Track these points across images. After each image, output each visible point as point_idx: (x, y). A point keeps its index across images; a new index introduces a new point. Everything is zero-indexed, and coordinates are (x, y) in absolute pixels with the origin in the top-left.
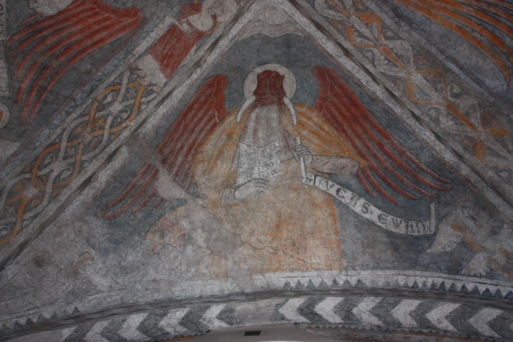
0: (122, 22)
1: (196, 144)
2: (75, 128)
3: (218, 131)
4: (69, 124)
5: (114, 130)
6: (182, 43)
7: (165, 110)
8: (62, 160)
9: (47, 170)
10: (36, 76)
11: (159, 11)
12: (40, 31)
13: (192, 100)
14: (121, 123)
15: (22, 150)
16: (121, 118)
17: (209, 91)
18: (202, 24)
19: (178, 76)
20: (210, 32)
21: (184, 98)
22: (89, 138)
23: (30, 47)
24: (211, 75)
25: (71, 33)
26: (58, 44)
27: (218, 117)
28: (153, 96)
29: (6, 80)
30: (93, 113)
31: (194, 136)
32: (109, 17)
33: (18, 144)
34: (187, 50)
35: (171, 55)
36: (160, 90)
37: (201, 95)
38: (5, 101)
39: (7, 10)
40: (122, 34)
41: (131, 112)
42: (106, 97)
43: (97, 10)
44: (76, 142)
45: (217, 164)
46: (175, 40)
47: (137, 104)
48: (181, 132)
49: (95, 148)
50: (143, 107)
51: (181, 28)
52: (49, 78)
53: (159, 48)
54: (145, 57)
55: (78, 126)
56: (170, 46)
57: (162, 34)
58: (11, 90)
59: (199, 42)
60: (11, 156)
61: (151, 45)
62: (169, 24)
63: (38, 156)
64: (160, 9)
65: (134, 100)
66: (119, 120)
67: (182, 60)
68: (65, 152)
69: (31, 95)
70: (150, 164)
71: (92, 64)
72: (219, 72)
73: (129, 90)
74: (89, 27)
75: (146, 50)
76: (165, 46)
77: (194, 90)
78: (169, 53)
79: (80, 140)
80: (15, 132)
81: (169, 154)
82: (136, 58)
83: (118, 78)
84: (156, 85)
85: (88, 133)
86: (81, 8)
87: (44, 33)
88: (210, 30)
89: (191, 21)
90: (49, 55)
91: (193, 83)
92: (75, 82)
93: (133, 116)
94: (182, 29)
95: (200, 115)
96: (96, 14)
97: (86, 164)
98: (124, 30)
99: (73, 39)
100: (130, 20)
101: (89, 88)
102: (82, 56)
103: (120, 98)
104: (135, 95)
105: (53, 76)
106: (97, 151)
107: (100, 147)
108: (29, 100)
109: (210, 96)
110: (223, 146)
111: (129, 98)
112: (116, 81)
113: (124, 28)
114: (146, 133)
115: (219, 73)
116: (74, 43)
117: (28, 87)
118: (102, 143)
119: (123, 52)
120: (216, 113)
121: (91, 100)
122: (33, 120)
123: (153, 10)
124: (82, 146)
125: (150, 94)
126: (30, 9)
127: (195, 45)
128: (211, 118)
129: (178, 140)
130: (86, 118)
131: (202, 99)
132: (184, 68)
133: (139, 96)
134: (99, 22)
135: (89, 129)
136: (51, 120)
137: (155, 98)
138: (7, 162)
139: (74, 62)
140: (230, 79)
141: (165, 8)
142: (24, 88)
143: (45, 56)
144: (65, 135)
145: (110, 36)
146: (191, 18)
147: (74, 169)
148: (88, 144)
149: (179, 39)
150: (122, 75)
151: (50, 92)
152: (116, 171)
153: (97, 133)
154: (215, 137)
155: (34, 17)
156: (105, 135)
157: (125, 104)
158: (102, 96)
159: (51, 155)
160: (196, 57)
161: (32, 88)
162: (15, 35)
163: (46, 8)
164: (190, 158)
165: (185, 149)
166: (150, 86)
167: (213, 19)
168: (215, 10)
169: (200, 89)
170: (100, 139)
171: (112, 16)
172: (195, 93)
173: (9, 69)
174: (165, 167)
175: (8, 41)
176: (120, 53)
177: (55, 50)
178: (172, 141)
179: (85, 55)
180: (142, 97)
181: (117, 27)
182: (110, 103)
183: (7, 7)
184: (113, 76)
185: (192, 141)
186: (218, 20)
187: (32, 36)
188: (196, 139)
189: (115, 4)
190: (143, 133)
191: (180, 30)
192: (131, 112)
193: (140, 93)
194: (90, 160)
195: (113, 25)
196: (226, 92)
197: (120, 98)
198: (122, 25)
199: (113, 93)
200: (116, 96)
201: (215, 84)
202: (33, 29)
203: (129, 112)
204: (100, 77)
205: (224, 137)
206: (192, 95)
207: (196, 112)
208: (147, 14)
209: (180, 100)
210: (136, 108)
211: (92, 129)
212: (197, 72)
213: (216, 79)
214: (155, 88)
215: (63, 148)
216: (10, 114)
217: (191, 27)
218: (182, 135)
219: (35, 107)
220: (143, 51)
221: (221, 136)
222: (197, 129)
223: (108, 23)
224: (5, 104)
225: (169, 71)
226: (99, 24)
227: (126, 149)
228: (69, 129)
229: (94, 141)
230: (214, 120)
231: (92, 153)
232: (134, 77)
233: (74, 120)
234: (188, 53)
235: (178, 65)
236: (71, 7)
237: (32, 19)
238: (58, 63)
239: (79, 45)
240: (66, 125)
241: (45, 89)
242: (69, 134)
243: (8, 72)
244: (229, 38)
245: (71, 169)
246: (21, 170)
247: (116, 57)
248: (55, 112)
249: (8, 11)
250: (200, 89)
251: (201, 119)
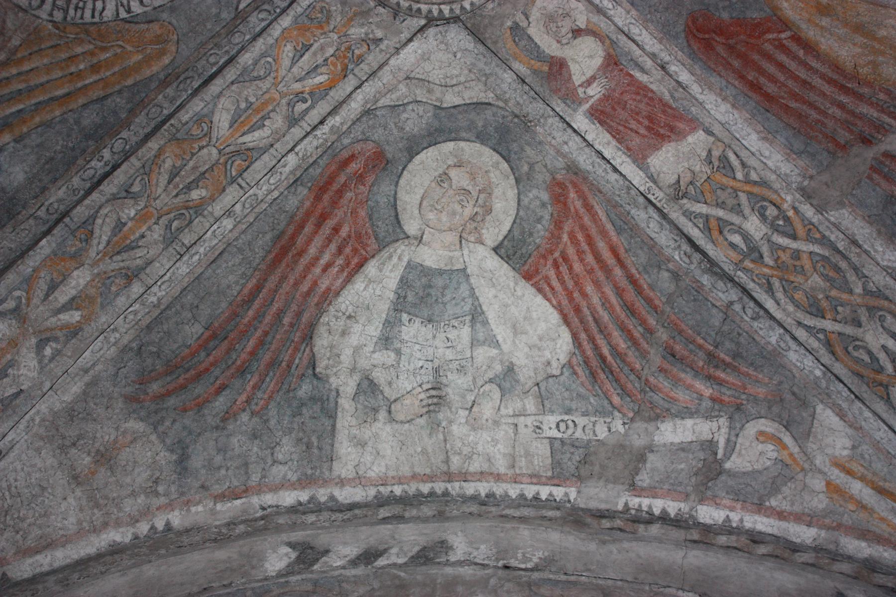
0: (576, 211)
1: (835, 77)
2: (797, 306)
3: (810, 33)
4: (788, 315)
5: (801, 232)
6: (626, 97)
7: (754, 136)
8: (861, 330)
9: (882, 356)
10: (688, 369)
11: (553, 141)
12: (603, 359)
13: (736, 83)
14: (787, 219)
15: (831, 401)
16: (777, 218)
17: (720, 49)
18: (591, 57)
19: (693, 109)
20: (608, 41)
21: (731, 99)
22: (816, 280)
23: (632, 377)
24: (685, 44)
25: (603, 304)
26: (623, 328)
27: (780, 32)
28: (732, 157)
29: (698, 421)
30: (766, 271)
31: (817, 81)
32: (569, 235)
33: (820, 408)
34: (642, 90)
35: (650, 118)
36: (720, 144)
37: (728, 65)
38: (738, 425)
39: (566, 414)
40: (599, 212)
41: (764, 199)
42: (733, 245)
43: (557, 254)
44: (824, 304)
45: (886, 37)
46: (619, 110)
47: (747, 188)
48: (805, 107)
49: (837, 269)
50: (754, 176)
51: (595, 98)
52: (691, 346)
53: (636, 142)
54: (652, 169)
55: (792, 299)
56: (632, 122)
57: (608, 136)
58: (717, 413)
59: (625, 64)
60: (845, 421)
61: (629, 156)
62: (587, 120)
63: (853, 372)
64: (549, 139)
65: (740, 193)
66: (781, 223)
67: (661, 100)
68: (846, 323)
69: (724, 381)
70: (870, 169)
71: (659, 268)
72: (680, 28)
73: (720, 201)
74: (591, 272)
75: (638, 166)
76: (631, 130)
77: (714, 79)
78: (646, 122)
79: (820, 296)
80: (795, 412)
81: (851, 132)
82: (654, 186)
83: (695, 221)
84: (710, 151)
85: (807, 280)
86: (555, 283)
87: (606, 351)
88: (603, 43)
89: (584, 79)
90: (646, 346)
91: (699, 81)
92: (695, 300)
93: (774, 197)
94: (598, 96)
95: (771, 69)
96: (565, 259)
97: (871, 287)
98: (592, 207)
99: (614, 299)
100: (572, 195)
101: (706, 276)
102: (645, 286)
103: (736, 219)
104: (730, 190)
105: (687, 339)
106: (843, 265)
107: (836, 259)
108: (733, 384)
109: (731, 48)
110: (846, 24)
111: (735, 202)
112: (701, 226)
113: (589, 208)
114: (799, 174)
115: (682, 27)
116: (622, 299)
117: (708, 384)
118: (827, 254)
119: (633, 212)
120: (770, 36)
121: (739, 273)
122: (771, 379)
123: (552, 152)
124: (834, 293)
125: (729, 162)
126: (562, 374)
127: (632, 72)
128: (782, 47)
129: (823, 113)
130: (776, 284)
131: (736, 63)
132: (676, 95)
133: (732, 183)
134: (580, 253)
135: (799, 279)
136: (770, 348)
137: (735, 154)
138: (856, 429)
139: (657, 302)
140: (696, 8)
141: (547, 128)
142: (711, 391)
143: (649, 353)
144: (810, 321)
145: (604, 233)
146: (577, 79)
147: (880, 309)
148: (828, 281)
149: (619, 103)
150: (688, 214)
151: (716, 347)
152: (879, 233)
153: (808, 266)
154: (823, 40)
155: (576, 368)
156: (812, 249)
157: (747, 211)
158: (732, 254)
159: (850, 348)
160: (655, 72)
161: (709, 377)
162: (611, 403)
163: (558, 346)
164: (865, 90)
165: (844, 99)
166: (711, 162)
167: (580, 35)
168: (564, 31)
169: (713, 66)
170: (818, 258)
171: (566, 229)
172: (721, 76)
173: (676, 416)
174: (880, 140)
175: (624, 415)
176: (636, 217)
177: (636, 334)
178: (823, 124)
179: (642, 281)
180: (734, 178)
181: (587, 220)
182: (746, 237)
183: (561, 414)
184: (691, 231)
185: (827, 86)
186: (583, 27)
187: (612, 372)
188: (823, 76)
189: (544, 222)
190: (799, 179)
191: (600, 100)
192: (764, 199)
193: (725, 180)
194: (863, 280)
195: (583, 228)
196: (725, 15)
197: (736, 219)
198: (582, 211)
199: (725, 232)
200: (730, 227)
201: (707, 36)
202: (599, 371)
203: (765, 203)
204: (682, 256)
205: (825, 22)
206: (724, 83)
207: (763, 75)
208: (560, 163)
209: (733, 106)
210: (756, 190)
211: (798, 273)
212: (676, 73)
213: (694, 35)
214: (716, 153)
215: (838, 327)
216: (761, 417)
217: (595, 78)
218: (811, 105)
219: (747, 375)
220: (641, 173)
221: (822, 28)
222: (802, 74)
223: (580, 237)
224: (743, 426)
225: (681, 125)
226: (583, 252)
227: (832, 213)
228: (798, 315)
229: (822, 269)
230: (784, 41)
231: (848, 275)
232: (693, 193)
233: (778, 304)
234: (646, 86)
235: (670, 107)
236: (554, 302)
237: (579, 371)
238: (662, 330)
239: (623, 290)
240: (789, 320)
241: (711, 356)
242: (809, 316)
243: (683, 418)
244: (610, 6)
245: (881, 313)
246: (882, 403)
247: (643, 225)
248: (754, 339)
249: (568, 411)
250: (713, 66)
251: (781, 66)
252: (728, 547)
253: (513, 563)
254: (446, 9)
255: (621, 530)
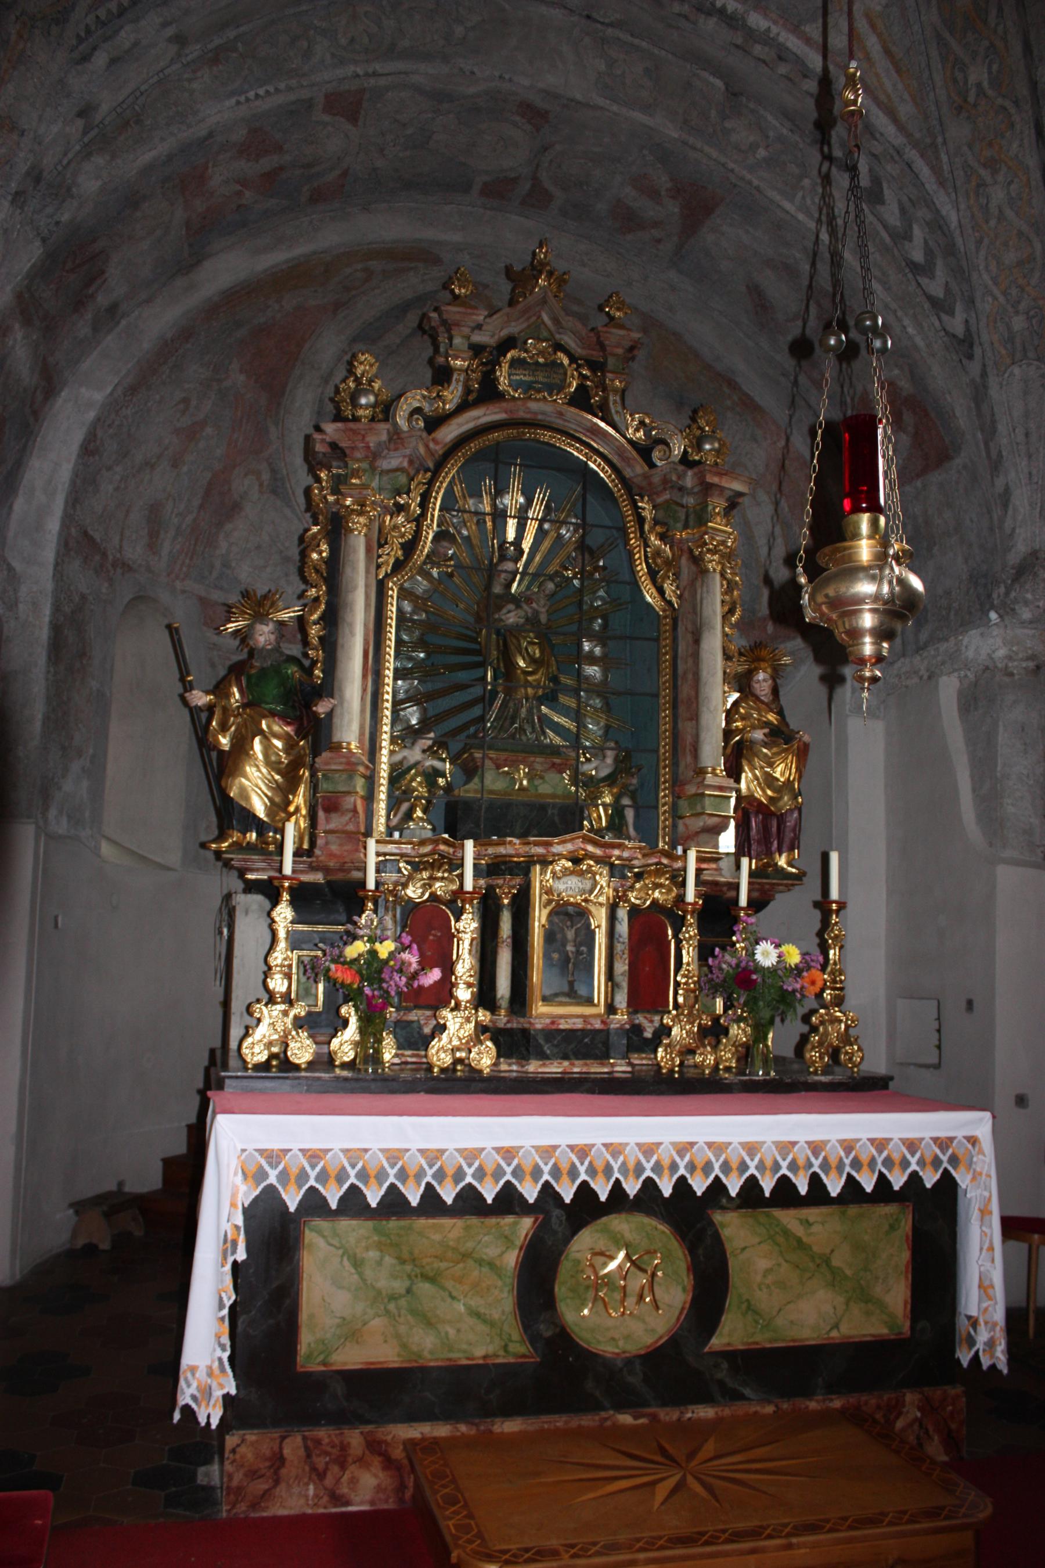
252: (759, 59)
253: (594, 15)
254: (102, 13)
255: (686, 17)
